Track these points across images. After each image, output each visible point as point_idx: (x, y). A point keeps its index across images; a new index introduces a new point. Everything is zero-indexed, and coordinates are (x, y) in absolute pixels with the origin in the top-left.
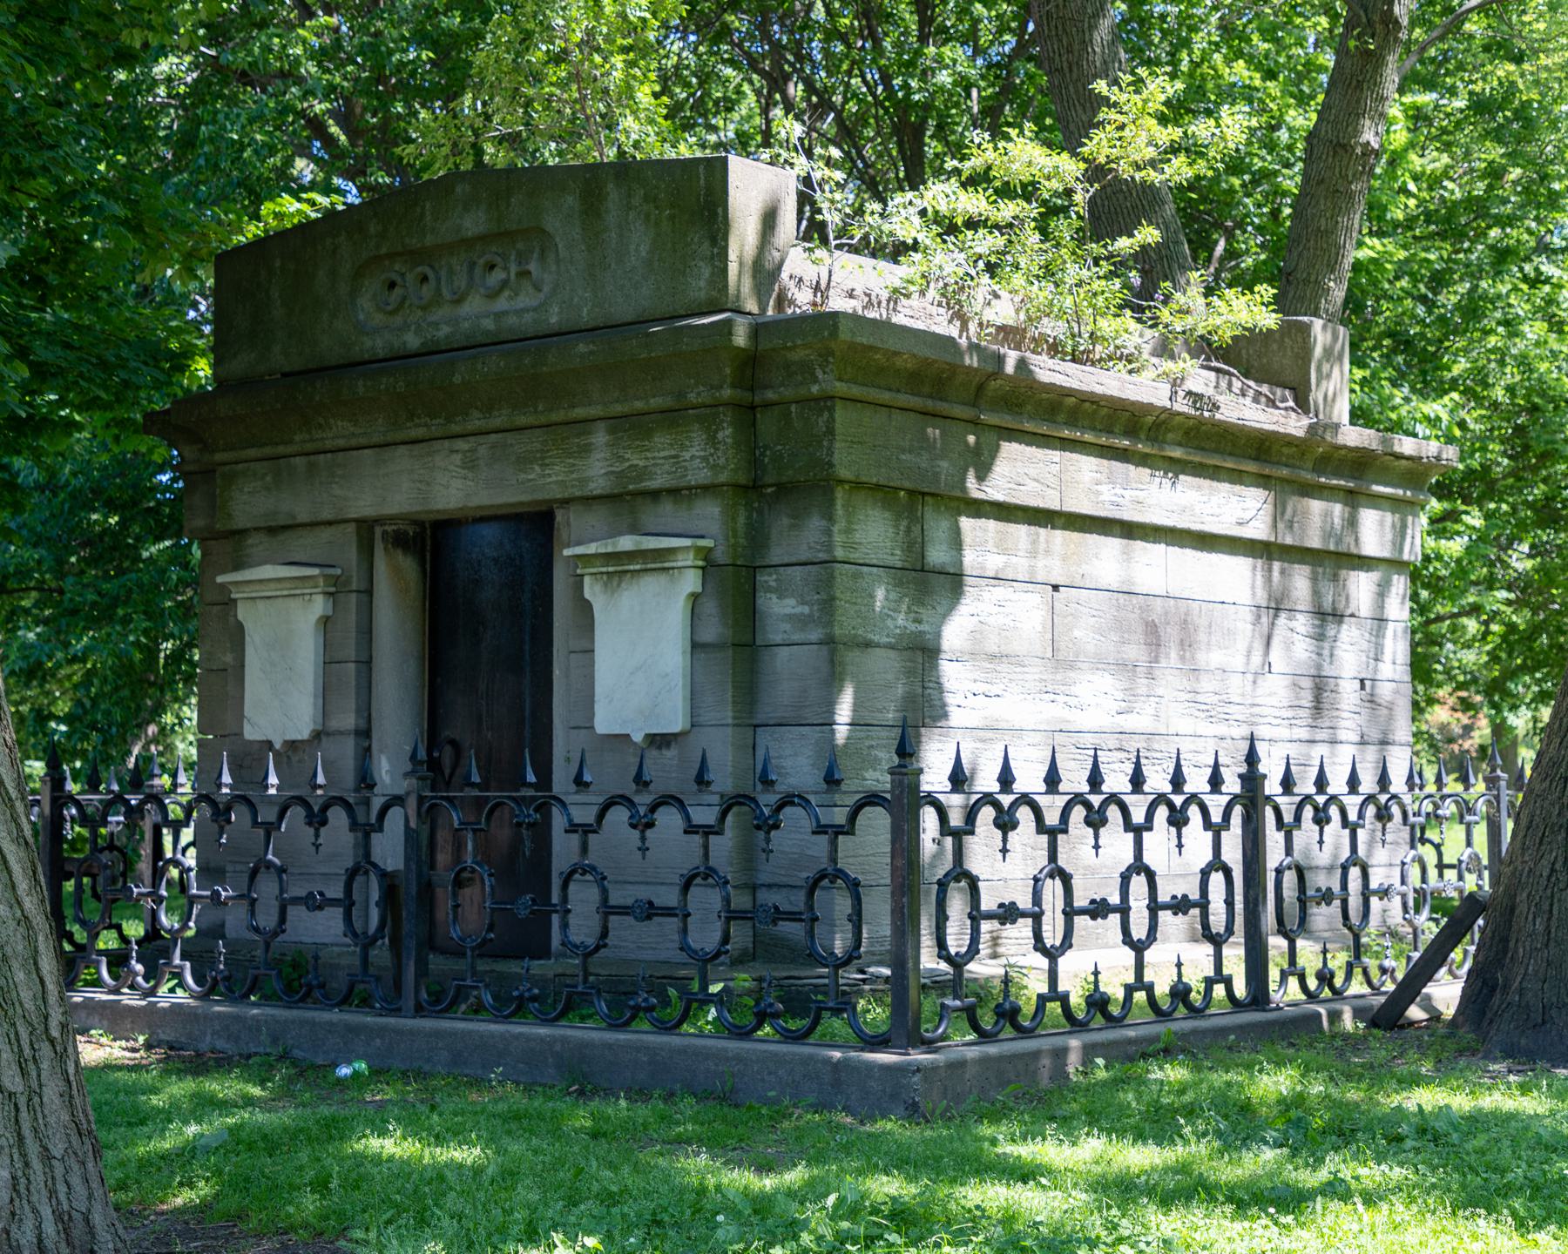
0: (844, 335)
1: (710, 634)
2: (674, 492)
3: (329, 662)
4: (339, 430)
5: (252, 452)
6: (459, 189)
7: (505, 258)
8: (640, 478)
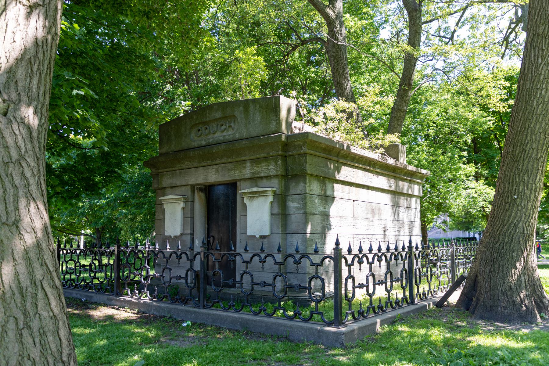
0: (310, 138)
1: (276, 211)
2: (266, 177)
3: (184, 218)
4: (186, 164)
5: (167, 170)
6: (215, 107)
7: (226, 123)
8: (258, 174)
